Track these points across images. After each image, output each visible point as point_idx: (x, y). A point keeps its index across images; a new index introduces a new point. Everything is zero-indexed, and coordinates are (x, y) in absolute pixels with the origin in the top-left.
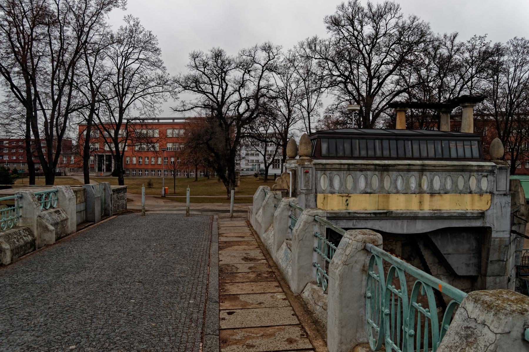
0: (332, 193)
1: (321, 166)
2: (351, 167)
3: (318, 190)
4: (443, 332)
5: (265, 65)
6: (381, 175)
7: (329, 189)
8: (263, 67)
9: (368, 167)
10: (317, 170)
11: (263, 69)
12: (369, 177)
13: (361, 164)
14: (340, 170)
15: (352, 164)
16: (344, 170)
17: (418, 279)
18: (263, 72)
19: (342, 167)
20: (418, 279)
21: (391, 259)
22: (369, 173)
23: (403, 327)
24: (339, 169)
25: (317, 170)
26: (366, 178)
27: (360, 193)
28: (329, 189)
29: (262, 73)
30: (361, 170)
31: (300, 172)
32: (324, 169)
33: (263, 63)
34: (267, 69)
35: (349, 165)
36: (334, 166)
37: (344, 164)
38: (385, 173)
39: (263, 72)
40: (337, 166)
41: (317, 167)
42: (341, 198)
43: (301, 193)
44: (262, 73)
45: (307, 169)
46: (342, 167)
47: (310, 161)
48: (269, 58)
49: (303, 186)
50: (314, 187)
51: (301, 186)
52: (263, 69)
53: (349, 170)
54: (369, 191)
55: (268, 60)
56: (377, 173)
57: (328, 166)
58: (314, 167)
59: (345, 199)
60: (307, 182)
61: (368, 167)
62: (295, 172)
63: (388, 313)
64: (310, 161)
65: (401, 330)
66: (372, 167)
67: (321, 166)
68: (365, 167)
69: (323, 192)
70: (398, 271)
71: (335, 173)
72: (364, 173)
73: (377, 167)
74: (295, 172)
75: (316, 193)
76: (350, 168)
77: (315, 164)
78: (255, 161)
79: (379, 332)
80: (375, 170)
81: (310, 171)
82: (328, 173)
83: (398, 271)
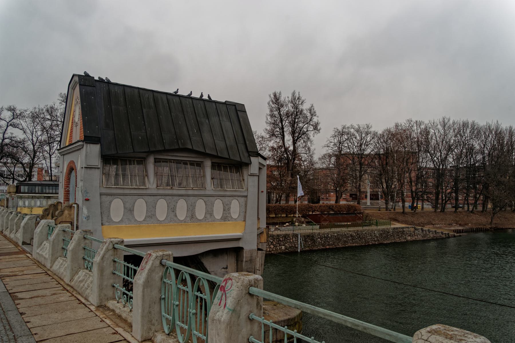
0: (25, 207)
1: (19, 197)
2: (33, 197)
3: (18, 206)
4: (212, 302)
5: (10, 121)
6: (47, 200)
7: (23, 206)
8: (8, 123)
9: (41, 197)
10: (18, 198)
11: (8, 124)
12: (42, 201)
13: (38, 196)
14: (28, 198)
15: (34, 196)
16: (30, 198)
17: (198, 277)
18: (8, 126)
19: (30, 197)
20: (198, 277)
21: (345, 318)
22: (41, 199)
23: (189, 309)
24: (28, 198)
25: (18, 198)
26: (40, 201)
27: (37, 207)
28: (23, 206)
29: (7, 127)
30: (38, 198)
31: (10, 199)
32: (21, 198)
33: (8, 120)
34: (11, 125)
35: (32, 196)
36: (26, 197)
37: (30, 196)
38: (49, 199)
39: (8, 126)
40: (27, 197)
41: (18, 197)
42: (28, 209)
43: (10, 207)
44: (7, 127)
45: (13, 198)
46: (30, 197)
47: (15, 195)
48: (14, 116)
49: (11, 204)
50: (16, 205)
51: (10, 204)
52: (8, 124)
53: (32, 198)
54: (41, 206)
55: (12, 118)
56: (45, 199)
57: (23, 197)
58: (16, 197)
59: (30, 209)
60: (13, 203)
61: (41, 197)
62: (8, 200)
63: (195, 312)
64: (15, 195)
65: (187, 311)
66: (43, 197)
67: (19, 197)
68: (40, 197)
69: (20, 207)
70: (203, 280)
71: (26, 199)
72: (39, 199)
73: (45, 197)
74: (8, 200)
75: (17, 207)
76: (33, 197)
77: (17, 196)
78: (5, 191)
79: (171, 320)
80: (44, 198)
81: (15, 198)
82: (23, 199)
83: (203, 280)
